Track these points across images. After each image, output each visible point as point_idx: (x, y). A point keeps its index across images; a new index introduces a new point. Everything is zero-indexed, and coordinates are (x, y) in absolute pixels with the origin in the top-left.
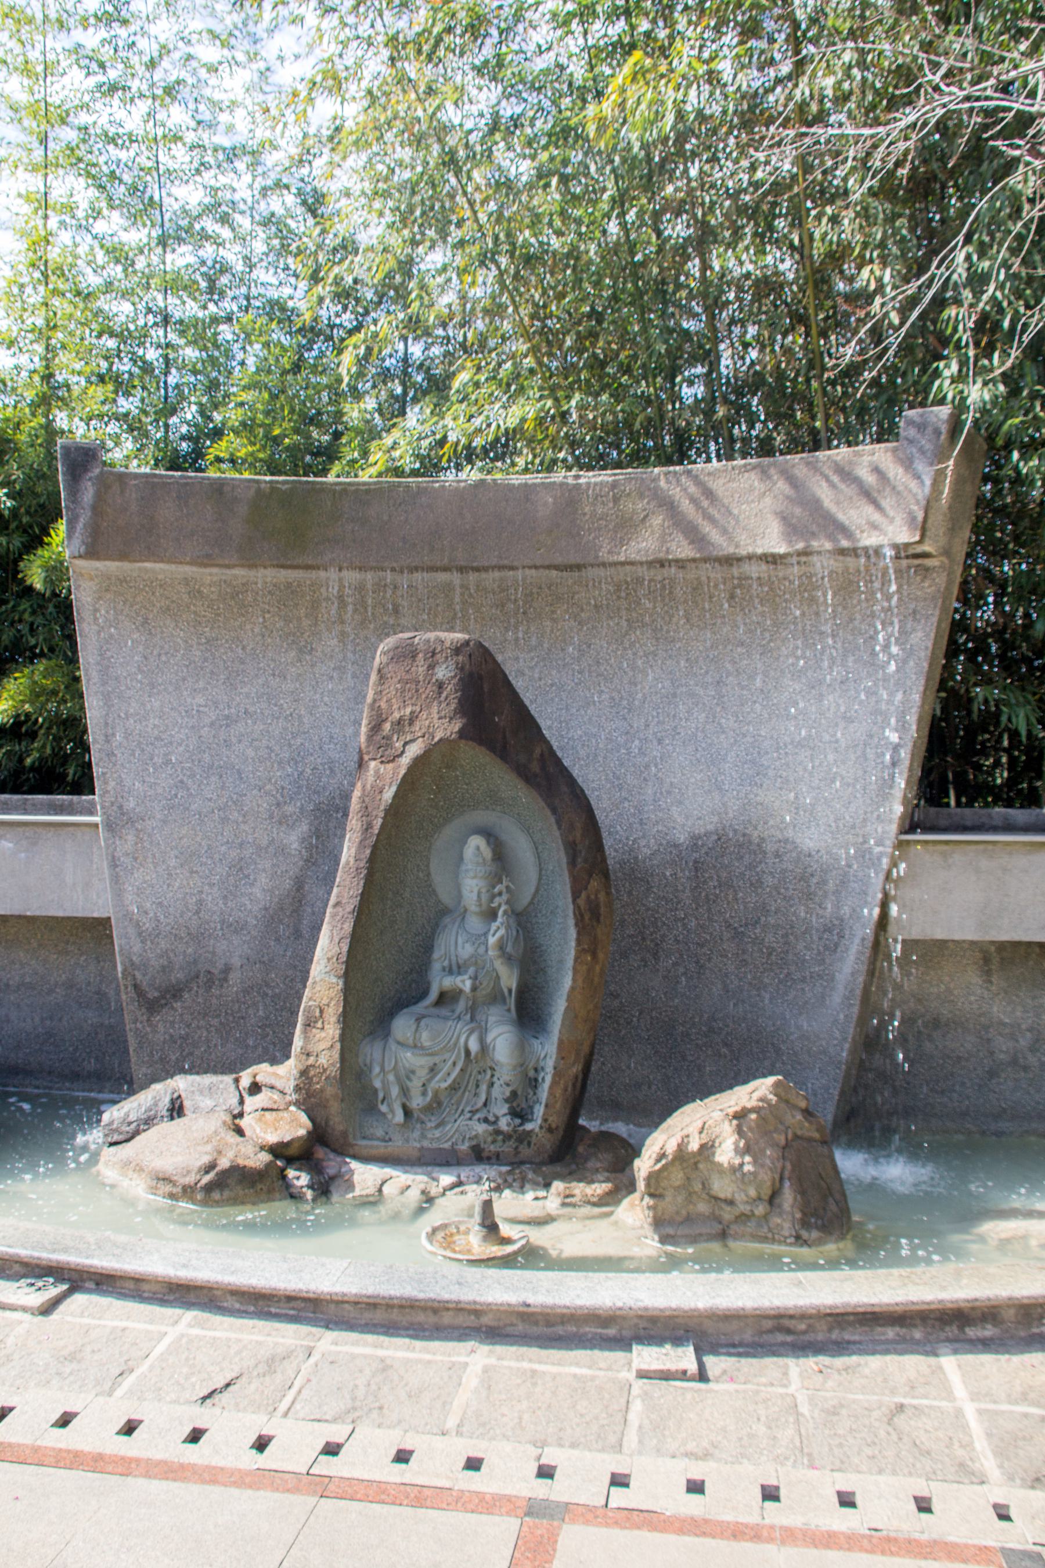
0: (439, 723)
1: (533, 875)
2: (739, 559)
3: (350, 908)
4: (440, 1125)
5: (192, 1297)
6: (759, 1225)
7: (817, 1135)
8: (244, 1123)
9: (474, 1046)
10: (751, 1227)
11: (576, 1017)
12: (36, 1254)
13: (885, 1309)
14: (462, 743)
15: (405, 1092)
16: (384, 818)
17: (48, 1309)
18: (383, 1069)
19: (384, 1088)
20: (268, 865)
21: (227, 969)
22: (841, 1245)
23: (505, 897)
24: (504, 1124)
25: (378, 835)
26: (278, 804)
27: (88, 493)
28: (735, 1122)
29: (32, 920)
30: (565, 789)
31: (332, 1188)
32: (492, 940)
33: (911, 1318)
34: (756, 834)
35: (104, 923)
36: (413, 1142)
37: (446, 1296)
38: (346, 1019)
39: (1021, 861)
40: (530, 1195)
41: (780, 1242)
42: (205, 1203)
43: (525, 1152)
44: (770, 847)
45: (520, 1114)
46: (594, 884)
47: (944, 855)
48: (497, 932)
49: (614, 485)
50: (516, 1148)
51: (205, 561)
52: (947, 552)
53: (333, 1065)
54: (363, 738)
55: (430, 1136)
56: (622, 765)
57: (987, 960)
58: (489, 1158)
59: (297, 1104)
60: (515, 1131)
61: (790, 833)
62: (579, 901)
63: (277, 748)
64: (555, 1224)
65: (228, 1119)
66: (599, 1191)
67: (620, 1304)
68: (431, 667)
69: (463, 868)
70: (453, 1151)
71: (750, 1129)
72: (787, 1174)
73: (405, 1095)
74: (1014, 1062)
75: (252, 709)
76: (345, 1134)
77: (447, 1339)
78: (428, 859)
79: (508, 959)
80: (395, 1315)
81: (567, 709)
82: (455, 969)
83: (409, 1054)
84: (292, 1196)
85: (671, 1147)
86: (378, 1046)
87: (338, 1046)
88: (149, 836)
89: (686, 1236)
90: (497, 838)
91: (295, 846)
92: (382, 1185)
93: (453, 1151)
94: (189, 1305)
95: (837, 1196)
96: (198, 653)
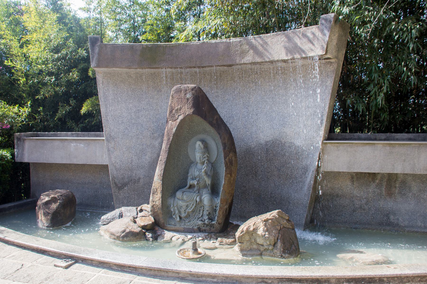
1: (216, 153)
2: (275, 62)
3: (164, 161)
5: (105, 265)
6: (271, 252)
7: (291, 227)
8: (137, 220)
9: (198, 200)
10: (268, 253)
11: (226, 192)
12: (67, 253)
13: (294, 278)
14: (194, 115)
15: (180, 212)
16: (173, 137)
17: (67, 267)
18: (173, 205)
20: (150, 150)
21: (139, 179)
22: (295, 259)
23: (206, 158)
24: (206, 222)
26: (153, 134)
27: (97, 50)
28: (264, 222)
29: (91, 165)
33: (303, 280)
34: (283, 141)
35: (106, 166)
37: (169, 268)
38: (163, 192)
39: (360, 148)
40: (212, 241)
41: (277, 257)
42: (123, 241)
43: (213, 230)
44: (287, 145)
45: (211, 219)
46: (231, 155)
47: (337, 147)
48: (204, 168)
49: (240, 42)
51: (129, 67)
52: (336, 57)
54: (168, 115)
56: (246, 122)
57: (352, 178)
58: (203, 231)
59: (151, 215)
61: (292, 141)
63: (152, 118)
64: (217, 250)
65: (132, 219)
66: (230, 241)
67: (217, 273)
68: (185, 94)
70: (193, 229)
71: (269, 225)
72: (279, 238)
74: (361, 207)
75: (145, 108)
76: (164, 223)
77: (170, 280)
80: (156, 273)
81: (231, 106)
84: (147, 240)
85: (245, 229)
86: (172, 199)
87: (161, 199)
88: (118, 142)
89: (250, 254)
93: (193, 229)
94: (104, 268)
95: (295, 245)
96: (130, 93)
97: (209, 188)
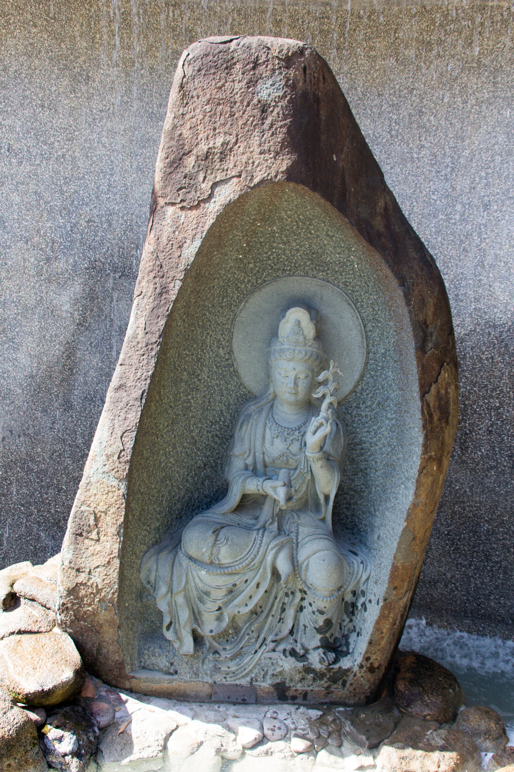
0: (260, 157)
4: (238, 655)
9: (283, 566)
11: (414, 539)
15: (196, 616)
16: (183, 281)
18: (170, 590)
19: (170, 612)
23: (331, 387)
25: (176, 301)
26: (48, 260)
30: (413, 254)
31: (102, 747)
32: (313, 440)
36: (203, 680)
38: (127, 531)
45: (335, 646)
48: (319, 430)
50: (329, 687)
53: (109, 585)
54: (158, 176)
55: (224, 668)
59: (63, 626)
60: (329, 670)
62: (427, 397)
63: (47, 195)
68: (252, 83)
69: (277, 347)
73: (196, 619)
75: (16, 146)
78: (231, 333)
79: (327, 458)
82: (262, 470)
83: (203, 572)
86: (165, 557)
87: (117, 563)
90: (317, 312)
91: (66, 307)
92: (166, 739)
97: (328, 512)
